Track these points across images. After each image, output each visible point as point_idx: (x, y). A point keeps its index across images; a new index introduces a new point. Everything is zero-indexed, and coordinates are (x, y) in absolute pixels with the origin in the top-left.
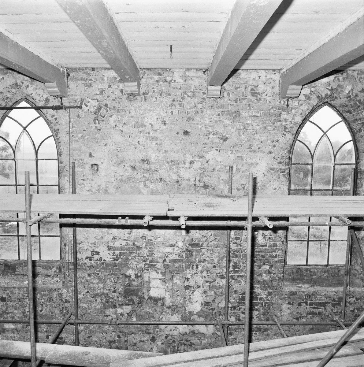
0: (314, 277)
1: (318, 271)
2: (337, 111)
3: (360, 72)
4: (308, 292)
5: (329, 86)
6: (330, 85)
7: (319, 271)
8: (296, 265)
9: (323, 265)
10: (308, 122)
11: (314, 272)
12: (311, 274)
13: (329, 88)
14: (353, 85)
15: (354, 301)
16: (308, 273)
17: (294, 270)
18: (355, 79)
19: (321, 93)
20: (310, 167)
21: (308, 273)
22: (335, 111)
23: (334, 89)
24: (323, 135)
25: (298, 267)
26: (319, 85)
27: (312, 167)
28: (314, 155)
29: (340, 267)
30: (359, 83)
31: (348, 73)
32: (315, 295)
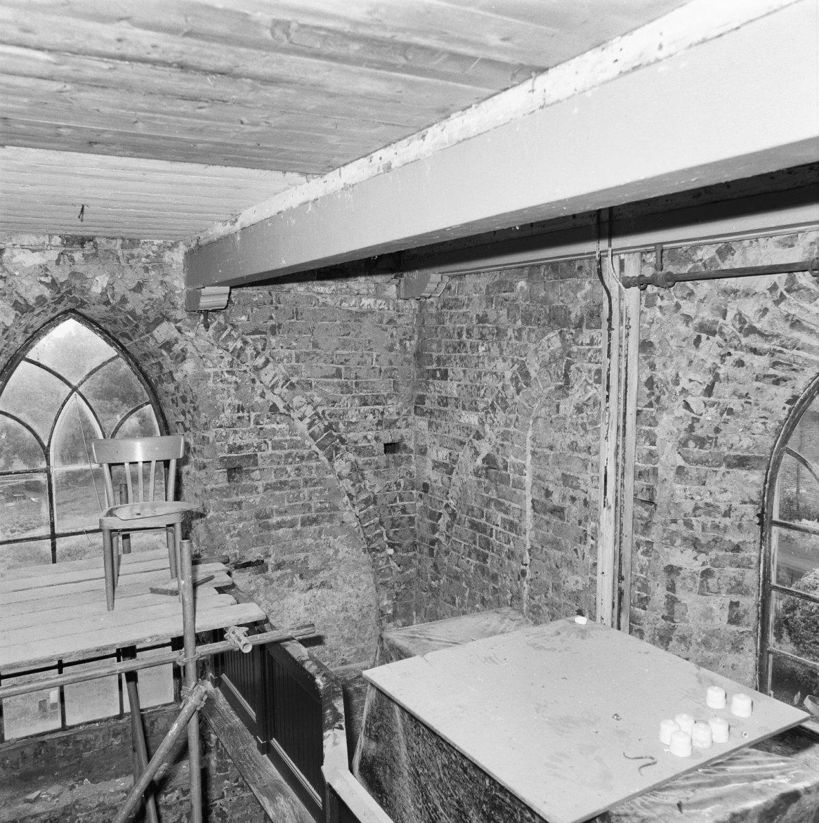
0: (86, 754)
1: (96, 737)
2: (101, 333)
3: (127, 241)
4: (50, 812)
5: (47, 276)
6: (48, 273)
7: (101, 735)
8: (32, 737)
9: (108, 719)
10: (23, 363)
11: (87, 741)
12: (78, 750)
13: (48, 280)
14: (112, 275)
15: (178, 798)
16: (70, 747)
17: (28, 751)
18: (118, 259)
19: (24, 295)
20: (42, 478)
21: (70, 747)
22: (96, 331)
23: (62, 284)
24: (71, 394)
25: (39, 739)
26: (17, 273)
27: (49, 477)
28: (49, 446)
29: (153, 712)
30: (128, 270)
31: (96, 243)
32: (70, 814)
